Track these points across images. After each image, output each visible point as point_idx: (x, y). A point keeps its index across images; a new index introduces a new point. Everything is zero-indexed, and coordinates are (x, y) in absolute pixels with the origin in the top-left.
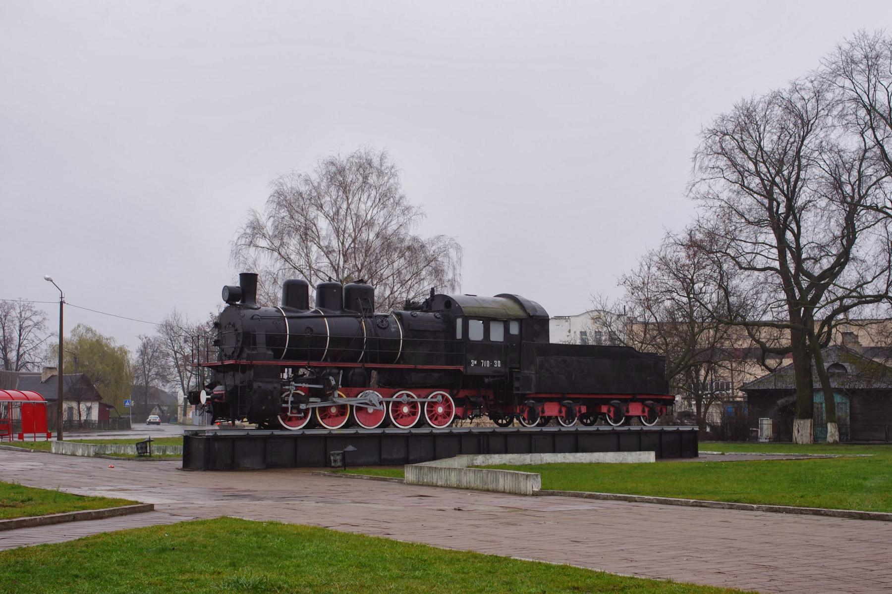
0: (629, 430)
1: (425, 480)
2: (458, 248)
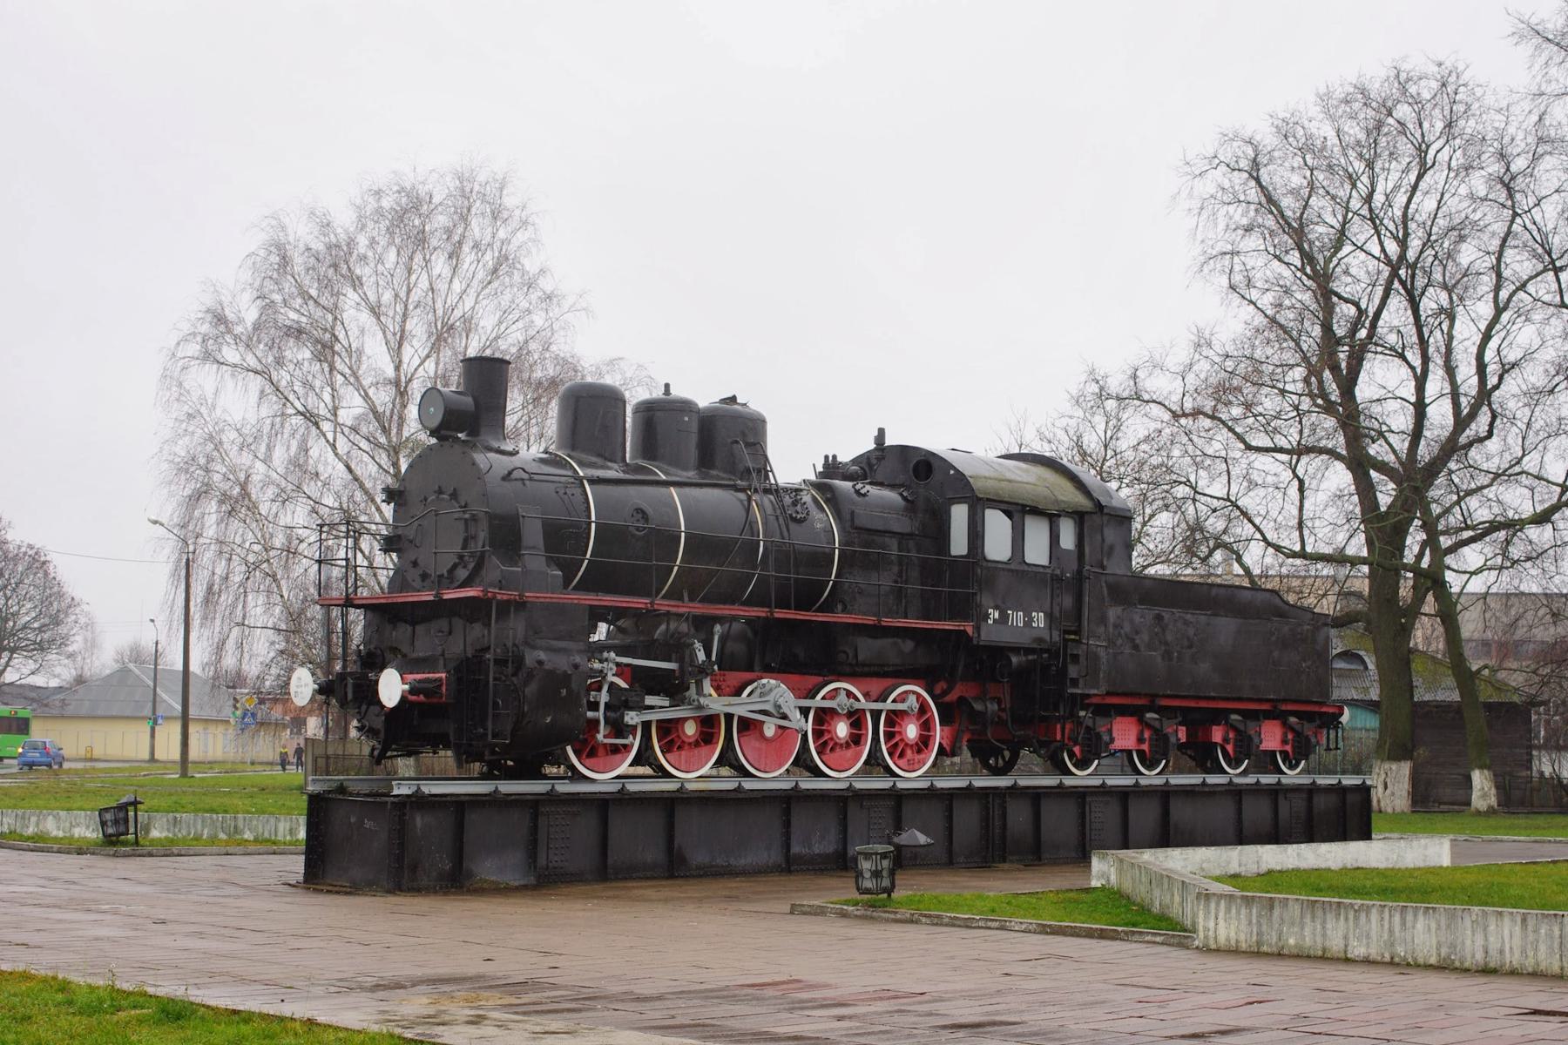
0: (1204, 784)
1: (1292, 941)
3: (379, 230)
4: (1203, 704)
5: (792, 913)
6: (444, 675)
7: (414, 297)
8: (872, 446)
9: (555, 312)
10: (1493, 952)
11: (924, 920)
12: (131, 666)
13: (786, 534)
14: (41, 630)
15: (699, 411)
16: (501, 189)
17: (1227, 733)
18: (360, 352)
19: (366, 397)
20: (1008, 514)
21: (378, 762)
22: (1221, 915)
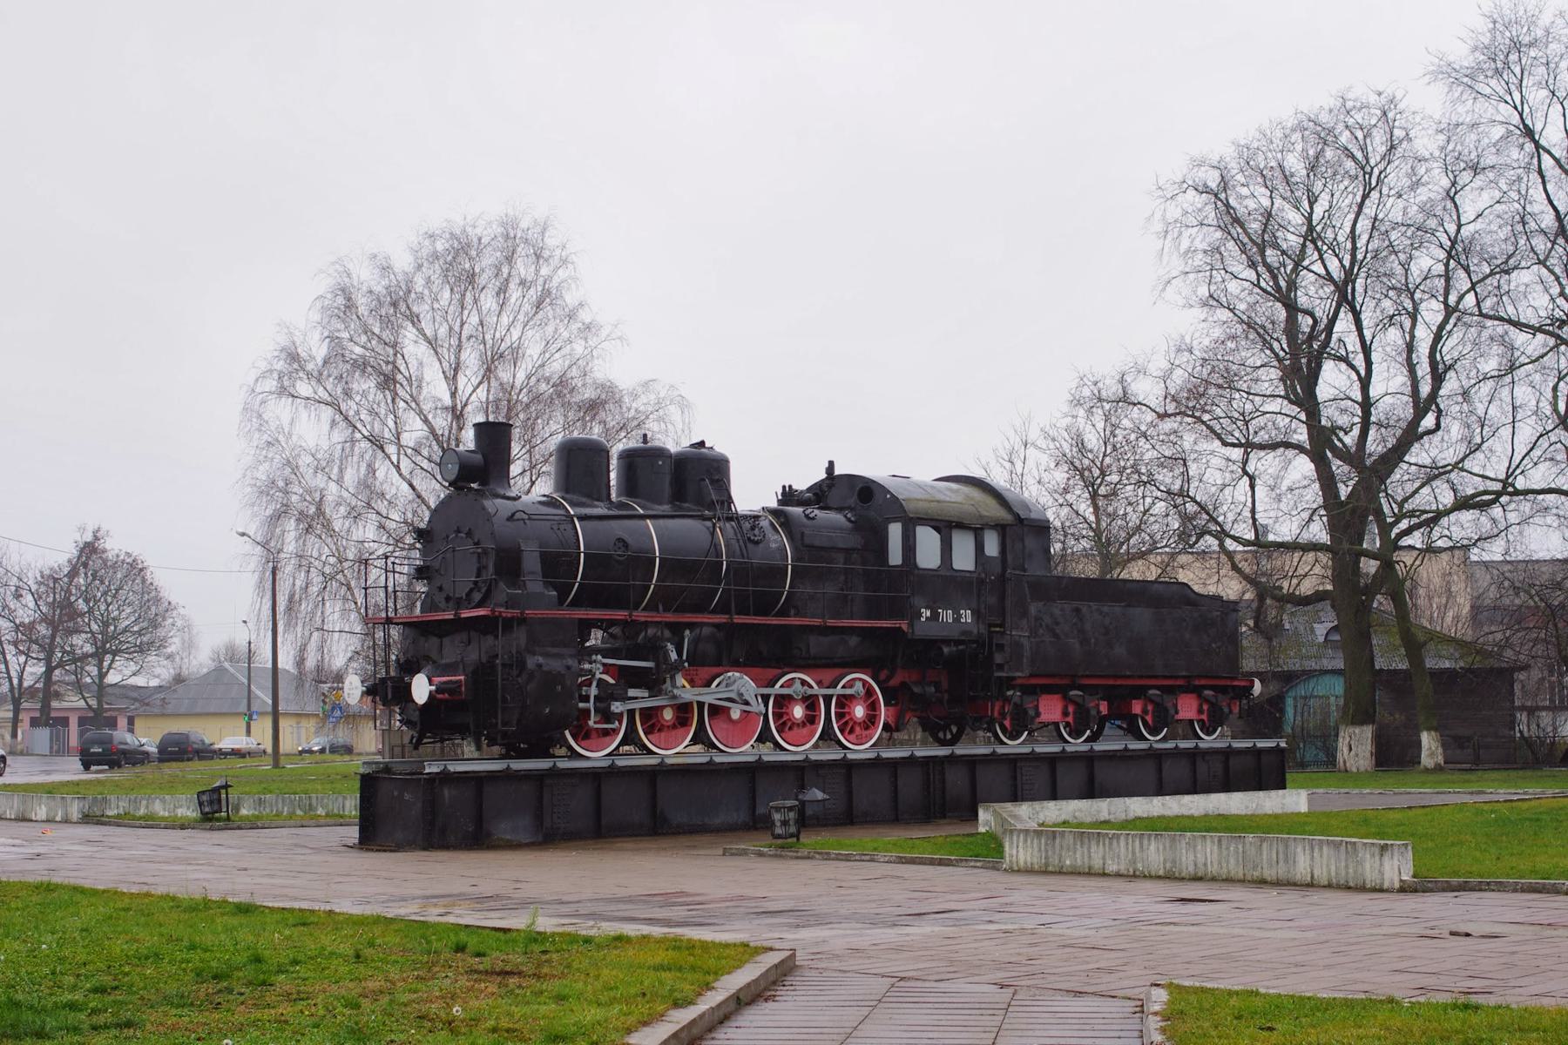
0: (1126, 749)
1: (1068, 862)
3: (435, 272)
5: (724, 855)
6: (462, 678)
10: (1200, 865)
11: (817, 856)
12: (227, 665)
13: (745, 555)
14: (140, 633)
15: (670, 456)
17: (1146, 705)
18: (420, 380)
19: (426, 421)
21: (416, 748)
22: (1021, 844)
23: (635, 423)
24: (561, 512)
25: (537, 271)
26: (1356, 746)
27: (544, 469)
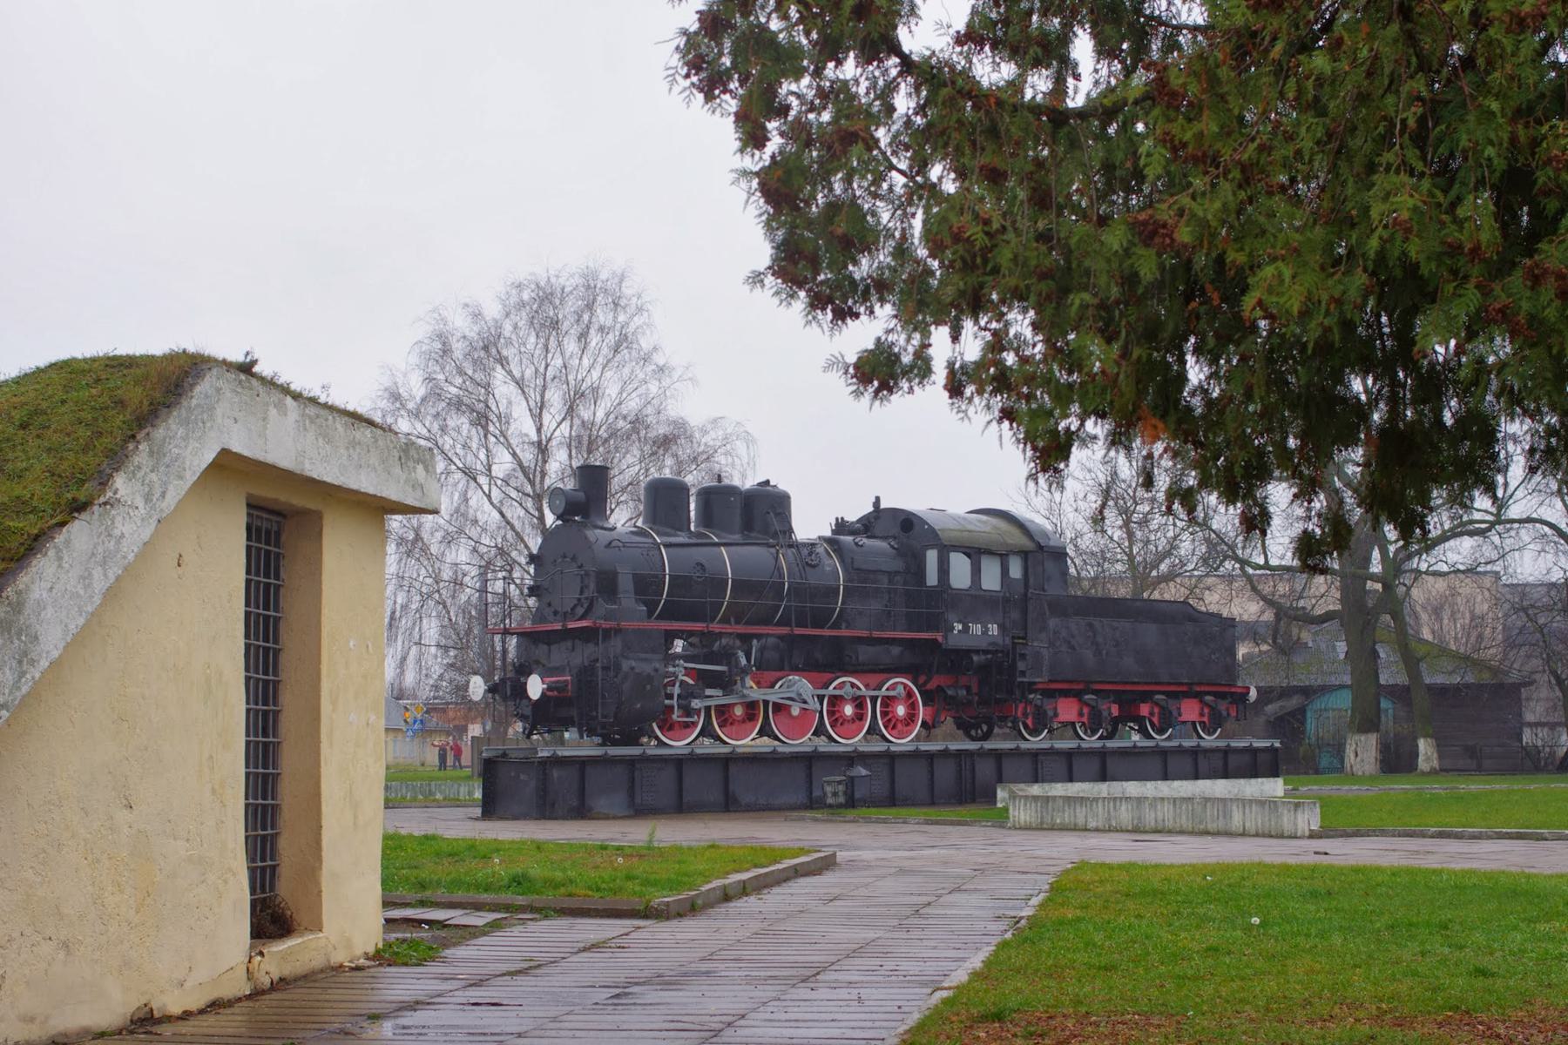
0: (1180, 746)
2: (749, 440)
4: (1128, 688)
7: (550, 374)
8: (871, 509)
9: (666, 382)
16: (621, 281)
19: (514, 455)
20: (969, 556)
23: (705, 457)
24: (650, 541)
25: (615, 318)
26: (1362, 752)
27: (622, 499)
